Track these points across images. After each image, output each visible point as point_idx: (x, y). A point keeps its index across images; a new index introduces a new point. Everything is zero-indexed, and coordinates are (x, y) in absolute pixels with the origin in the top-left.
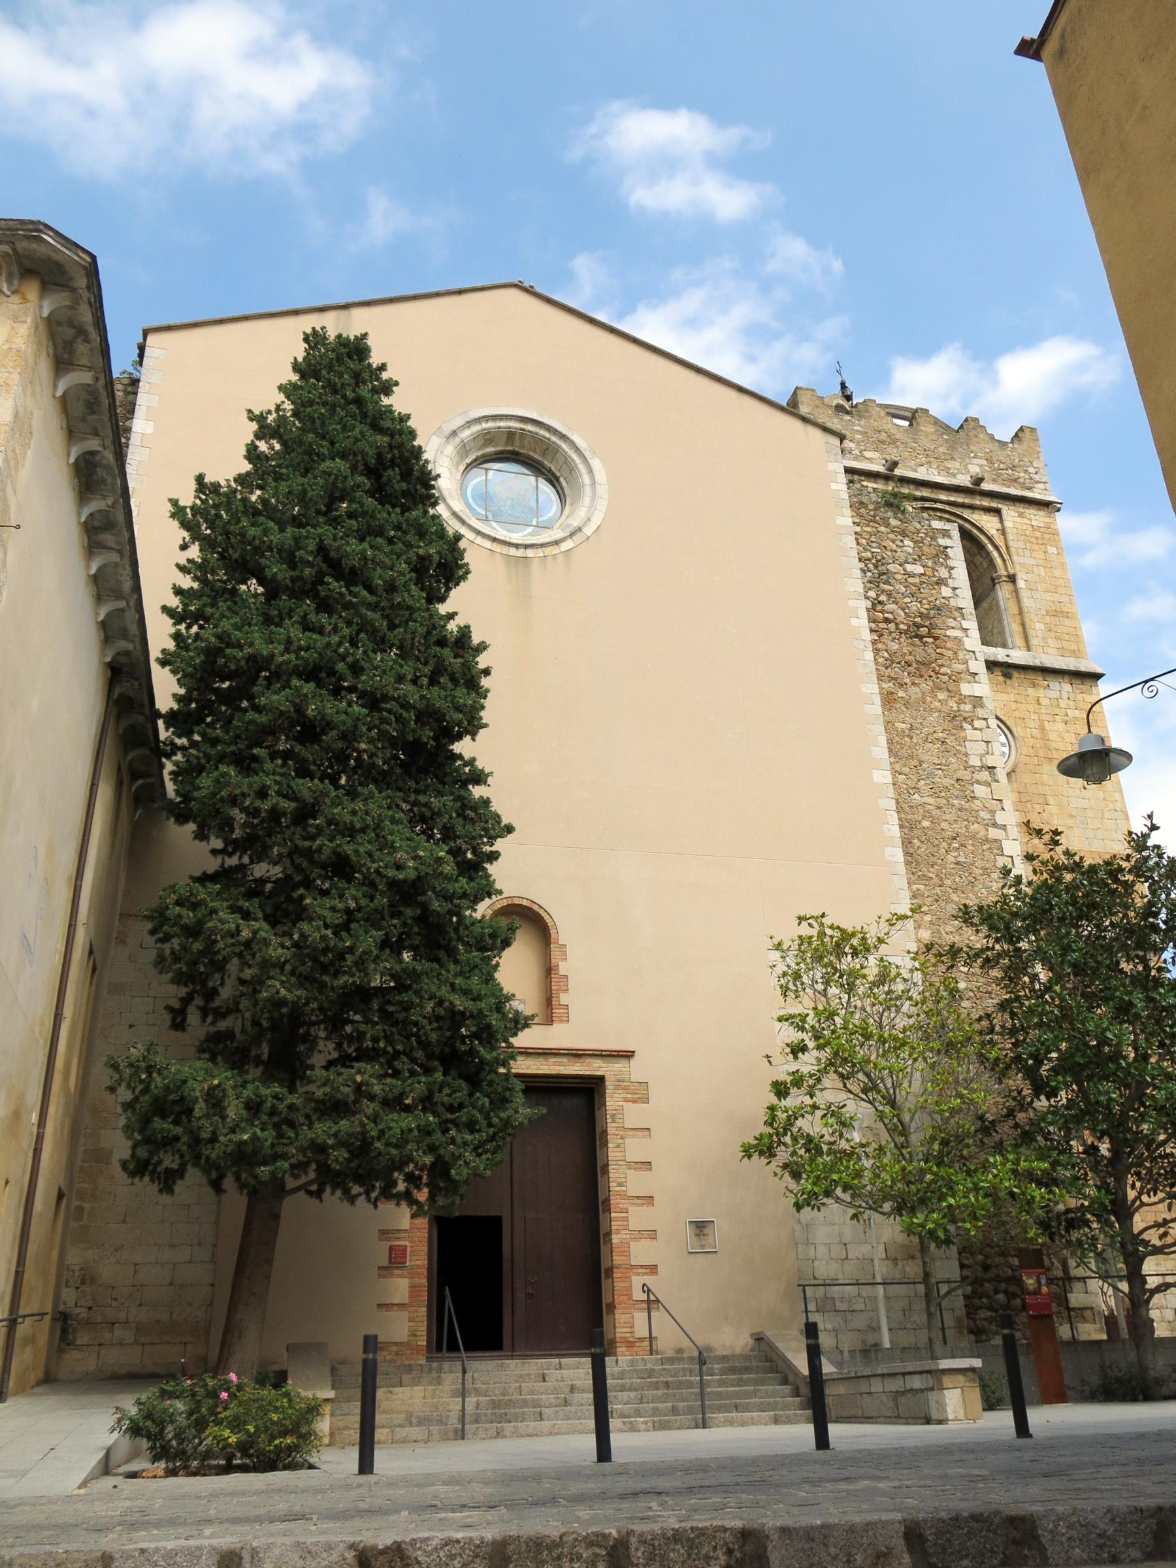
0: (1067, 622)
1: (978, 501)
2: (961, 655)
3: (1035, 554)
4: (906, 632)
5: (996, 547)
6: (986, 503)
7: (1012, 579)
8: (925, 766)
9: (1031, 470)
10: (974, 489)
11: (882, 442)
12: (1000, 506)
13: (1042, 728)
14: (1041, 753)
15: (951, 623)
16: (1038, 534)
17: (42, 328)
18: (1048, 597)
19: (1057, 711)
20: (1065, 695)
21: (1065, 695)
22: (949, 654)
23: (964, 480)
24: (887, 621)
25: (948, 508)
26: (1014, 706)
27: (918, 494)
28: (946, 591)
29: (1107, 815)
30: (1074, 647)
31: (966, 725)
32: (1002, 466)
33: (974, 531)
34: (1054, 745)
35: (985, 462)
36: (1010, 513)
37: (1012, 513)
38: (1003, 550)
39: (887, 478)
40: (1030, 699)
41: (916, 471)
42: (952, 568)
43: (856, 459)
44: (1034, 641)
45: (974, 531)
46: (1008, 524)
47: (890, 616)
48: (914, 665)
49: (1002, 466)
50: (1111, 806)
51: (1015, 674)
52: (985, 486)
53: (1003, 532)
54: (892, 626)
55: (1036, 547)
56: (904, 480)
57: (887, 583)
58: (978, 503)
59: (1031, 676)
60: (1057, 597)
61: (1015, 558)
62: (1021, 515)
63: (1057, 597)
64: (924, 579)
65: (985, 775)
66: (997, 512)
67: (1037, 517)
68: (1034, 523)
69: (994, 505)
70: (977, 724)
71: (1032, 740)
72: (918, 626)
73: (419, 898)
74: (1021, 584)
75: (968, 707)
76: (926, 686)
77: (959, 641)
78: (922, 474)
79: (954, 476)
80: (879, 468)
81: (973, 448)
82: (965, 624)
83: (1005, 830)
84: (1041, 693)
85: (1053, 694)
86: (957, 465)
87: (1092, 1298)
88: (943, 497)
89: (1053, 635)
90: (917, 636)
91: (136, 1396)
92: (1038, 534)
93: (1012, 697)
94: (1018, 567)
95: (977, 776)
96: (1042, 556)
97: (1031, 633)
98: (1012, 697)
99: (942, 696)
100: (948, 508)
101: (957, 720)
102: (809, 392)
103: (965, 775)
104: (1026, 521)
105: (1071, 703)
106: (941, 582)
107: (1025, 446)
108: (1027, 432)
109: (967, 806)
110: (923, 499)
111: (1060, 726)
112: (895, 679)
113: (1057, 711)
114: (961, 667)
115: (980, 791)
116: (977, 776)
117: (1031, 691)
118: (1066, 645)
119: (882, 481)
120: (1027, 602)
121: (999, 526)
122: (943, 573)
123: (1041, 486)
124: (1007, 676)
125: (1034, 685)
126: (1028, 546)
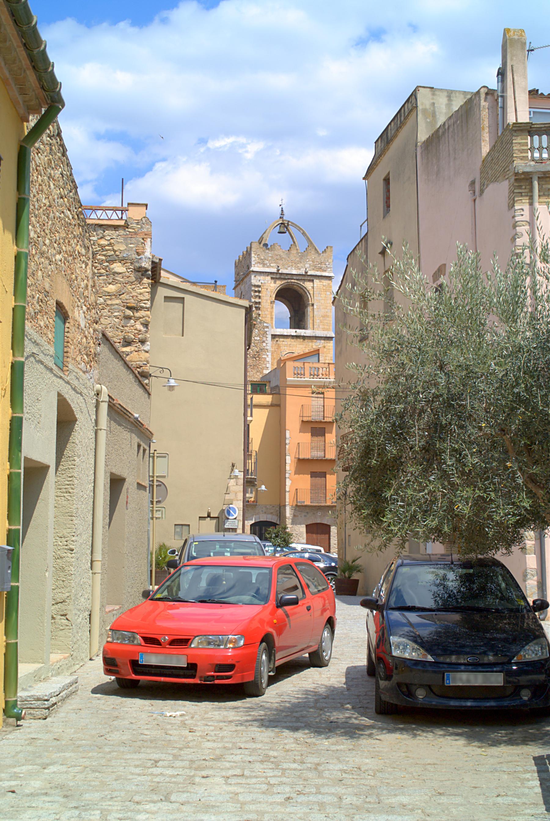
0: (328, 319)
3: (322, 295)
5: (310, 294)
7: (313, 305)
9: (327, 263)
16: (324, 288)
17: (379, 716)
18: (323, 310)
22: (262, 362)
25: (296, 281)
28: (264, 344)
30: (328, 327)
36: (316, 281)
38: (312, 295)
43: (268, 267)
44: (315, 327)
46: (315, 285)
53: (313, 287)
56: (281, 274)
61: (315, 298)
67: (325, 282)
69: (311, 279)
73: (291, 545)
74: (315, 307)
76: (254, 371)
77: (265, 358)
81: (308, 257)
82: (268, 354)
86: (302, 265)
92: (324, 288)
96: (324, 295)
97: (315, 324)
99: (258, 374)
100: (296, 281)
106: (264, 342)
107: (327, 254)
108: (329, 248)
114: (264, 366)
117: (310, 344)
118: (326, 327)
120: (315, 313)
121: (312, 285)
122: (264, 339)
124: (304, 340)
125: (312, 342)
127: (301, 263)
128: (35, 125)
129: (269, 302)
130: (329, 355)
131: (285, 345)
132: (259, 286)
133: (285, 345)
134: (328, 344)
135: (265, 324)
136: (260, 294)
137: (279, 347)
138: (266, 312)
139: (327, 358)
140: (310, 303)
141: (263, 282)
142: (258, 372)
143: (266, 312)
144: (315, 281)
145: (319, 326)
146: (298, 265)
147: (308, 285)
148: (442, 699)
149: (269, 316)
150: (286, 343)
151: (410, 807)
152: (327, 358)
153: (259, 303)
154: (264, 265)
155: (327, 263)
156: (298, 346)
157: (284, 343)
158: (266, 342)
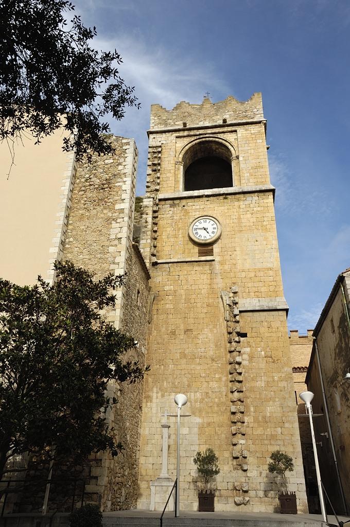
0: (262, 170)
1: (226, 129)
2: (119, 193)
3: (250, 145)
4: (97, 188)
6: (230, 129)
7: (238, 157)
8: (88, 242)
10: (225, 124)
11: (185, 117)
12: (236, 129)
13: (239, 218)
14: (236, 229)
15: (119, 180)
19: (248, 209)
20: (254, 202)
21: (254, 202)
22: (114, 193)
23: (221, 122)
24: (91, 185)
25: (211, 135)
26: (226, 211)
27: (198, 133)
28: (120, 167)
29: (266, 251)
30: (263, 180)
31: (113, 222)
32: (240, 112)
33: (224, 142)
34: (244, 224)
35: (232, 113)
36: (240, 130)
37: (242, 130)
38: (235, 145)
39: (183, 130)
40: (236, 207)
41: (198, 124)
42: (126, 157)
43: (172, 126)
45: (224, 142)
47: (92, 183)
48: (97, 201)
49: (240, 112)
50: (269, 247)
51: (229, 197)
52: (228, 122)
54: (92, 187)
55: (252, 142)
56: (190, 129)
57: (95, 170)
58: (226, 130)
59: (238, 196)
60: (259, 160)
62: (246, 130)
63: (259, 160)
64: (112, 165)
65: (116, 242)
66: (236, 131)
68: (252, 132)
70: (118, 221)
71: (233, 224)
72: (103, 184)
74: (241, 158)
75: (116, 214)
78: (201, 124)
79: (216, 122)
80: (181, 127)
82: (125, 179)
83: (118, 265)
84: (241, 203)
85: (247, 203)
87: (99, 488)
88: (209, 131)
89: (253, 177)
90: (102, 189)
91: (296, 453)
92: (253, 136)
93: (226, 207)
94: (240, 152)
95: (112, 243)
98: (226, 207)
99: (105, 211)
100: (211, 135)
101: (109, 221)
102: (155, 106)
103: (107, 243)
104: (248, 132)
105: (257, 205)
106: (120, 164)
109: (103, 257)
110: (200, 135)
111: (249, 216)
112: (86, 208)
113: (248, 209)
114: (117, 198)
115: (111, 249)
116: (112, 243)
117: (236, 203)
119: (182, 132)
123: (259, 115)
126: (247, 142)
127: (217, 115)
128: (144, 263)
129: (172, 162)
130: (267, 214)
131: (196, 210)
132: (160, 147)
133: (196, 210)
134: (265, 201)
135: (124, 141)
136: (160, 155)
137: (187, 212)
138: (168, 175)
139: (265, 219)
140: (234, 156)
141: (164, 142)
142: (105, 208)
143: (168, 175)
144: (238, 131)
145: (248, 180)
146: (213, 118)
147: (230, 137)
148: (189, 195)
149: (172, 178)
150: (198, 207)
151: (275, 269)
152: (265, 219)
153: (159, 164)
154: (166, 125)
155: (256, 110)
156: (216, 208)
157: (194, 207)
158: (124, 164)
